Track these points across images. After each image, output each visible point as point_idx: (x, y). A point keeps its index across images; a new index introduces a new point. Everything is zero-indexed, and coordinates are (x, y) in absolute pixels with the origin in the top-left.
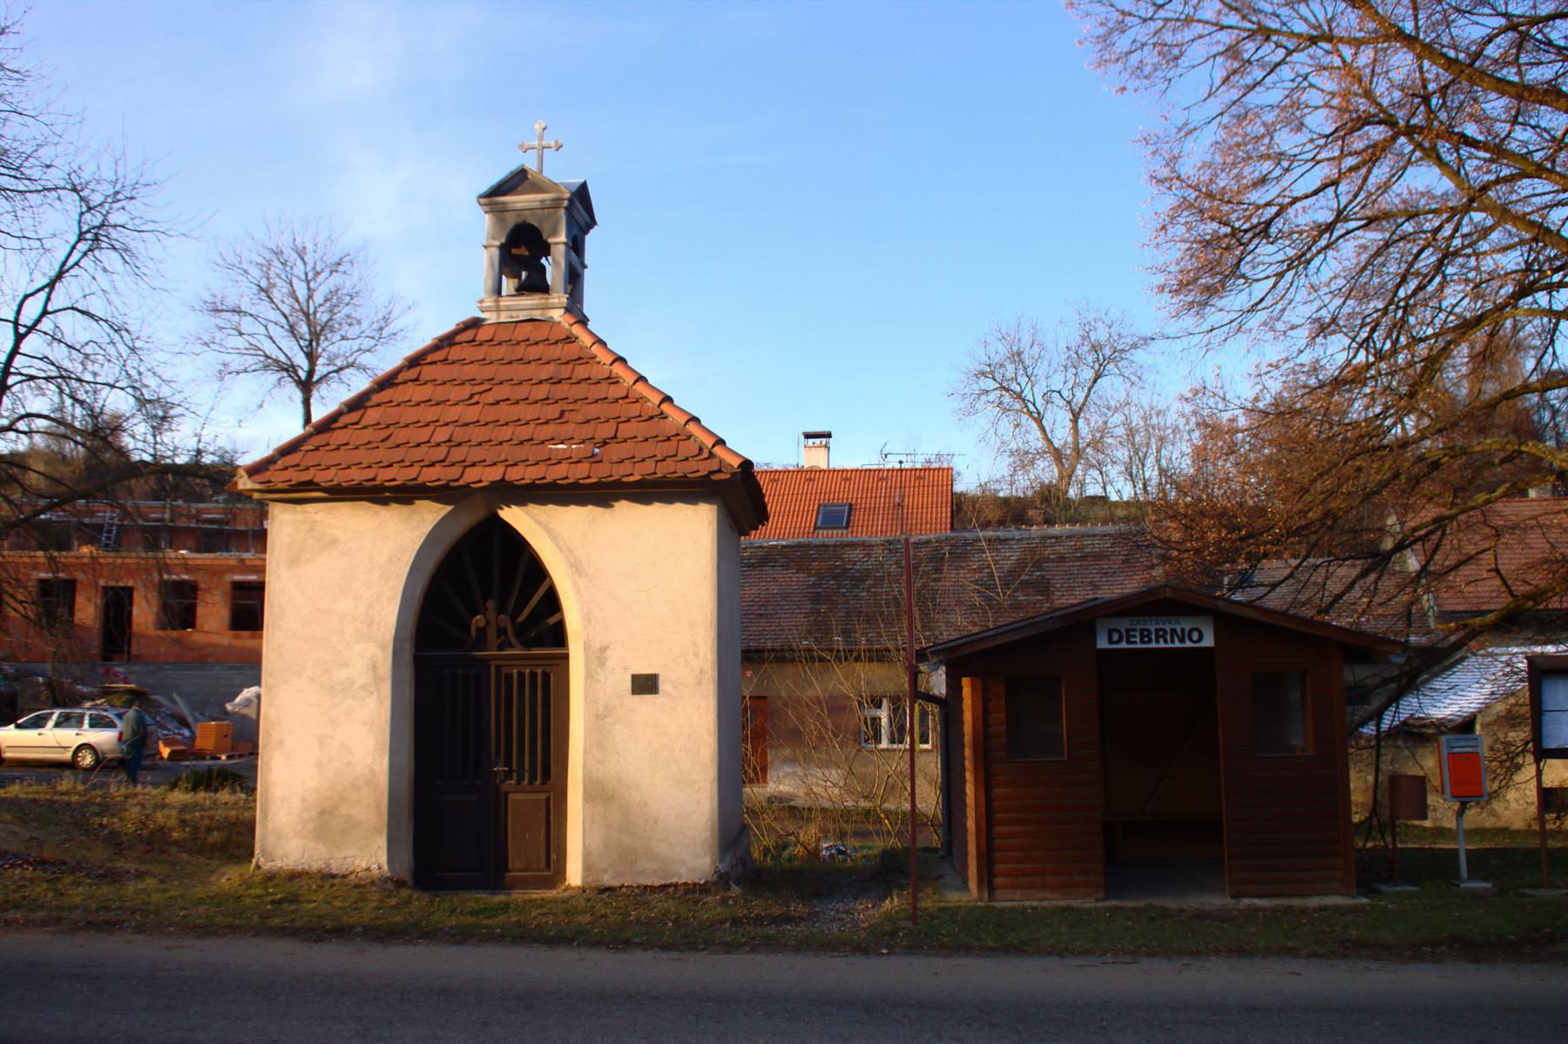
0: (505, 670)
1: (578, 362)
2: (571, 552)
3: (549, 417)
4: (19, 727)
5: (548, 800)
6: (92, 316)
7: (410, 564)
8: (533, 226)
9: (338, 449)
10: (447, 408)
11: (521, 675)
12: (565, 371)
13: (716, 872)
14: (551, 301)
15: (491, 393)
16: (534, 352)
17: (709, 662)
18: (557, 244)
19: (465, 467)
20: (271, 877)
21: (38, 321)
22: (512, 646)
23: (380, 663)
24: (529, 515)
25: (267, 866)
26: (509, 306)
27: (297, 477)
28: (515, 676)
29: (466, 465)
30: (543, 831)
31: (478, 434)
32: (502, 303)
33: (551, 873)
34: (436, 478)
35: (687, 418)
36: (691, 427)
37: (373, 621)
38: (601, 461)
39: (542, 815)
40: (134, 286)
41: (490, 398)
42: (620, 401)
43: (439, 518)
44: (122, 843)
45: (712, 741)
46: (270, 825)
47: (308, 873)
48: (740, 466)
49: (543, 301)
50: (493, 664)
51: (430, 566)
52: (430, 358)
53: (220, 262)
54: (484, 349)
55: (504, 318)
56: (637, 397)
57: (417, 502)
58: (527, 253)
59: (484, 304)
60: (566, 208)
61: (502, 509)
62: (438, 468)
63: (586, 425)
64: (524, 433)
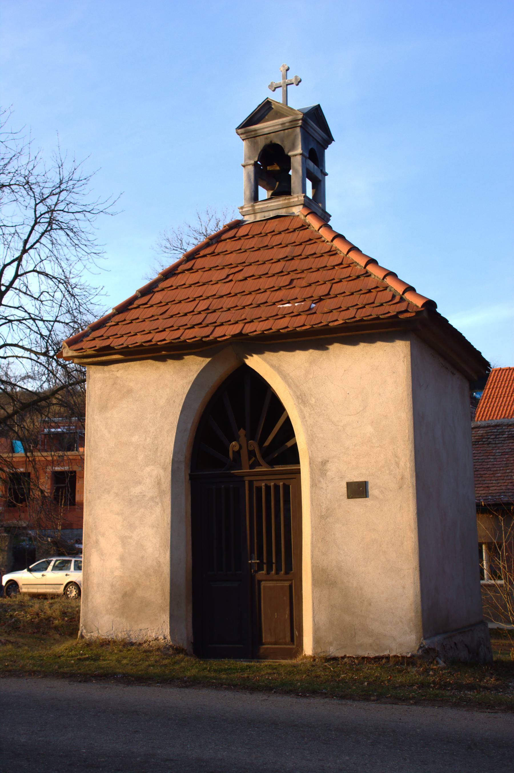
0: (256, 484)
1: (308, 243)
2: (297, 386)
3: (282, 284)
4: (30, 570)
5: (291, 586)
6: (47, 275)
7: (182, 405)
8: (278, 145)
9: (131, 322)
10: (210, 286)
11: (268, 488)
12: (298, 250)
13: (420, 647)
14: (292, 200)
15: (242, 272)
16: (277, 240)
17: (408, 470)
18: (296, 155)
19: (216, 327)
20: (89, 644)
21: (12, 282)
22: (260, 465)
23: (163, 481)
24: (265, 360)
25: (87, 637)
26: (262, 208)
27: (99, 344)
28: (263, 488)
29: (216, 325)
30: (288, 612)
31: (228, 302)
32: (256, 207)
33: (294, 646)
34: (194, 336)
35: (385, 273)
36: (389, 281)
37: (157, 449)
38: (315, 313)
39: (286, 599)
40: (74, 252)
41: (241, 276)
42: (336, 268)
43: (202, 368)
44: (19, 627)
45: (413, 536)
46: (90, 605)
47: (115, 642)
48: (423, 306)
49: (286, 201)
50: (247, 479)
51: (197, 406)
52: (202, 253)
53: (168, 245)
54: (241, 242)
55: (259, 217)
56: (349, 263)
57: (186, 357)
58: (278, 168)
59: (244, 210)
60: (301, 126)
61: (247, 358)
62: (197, 329)
63: (308, 288)
64: (261, 298)
